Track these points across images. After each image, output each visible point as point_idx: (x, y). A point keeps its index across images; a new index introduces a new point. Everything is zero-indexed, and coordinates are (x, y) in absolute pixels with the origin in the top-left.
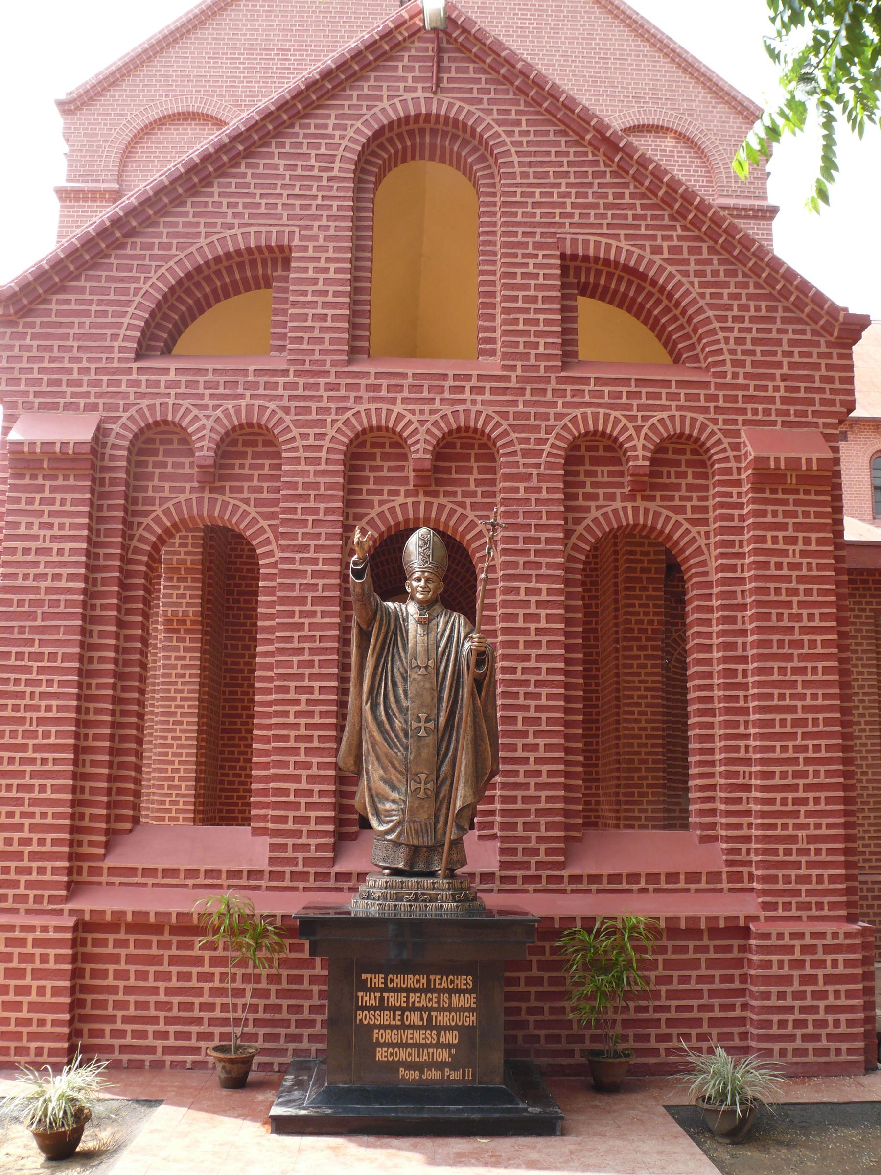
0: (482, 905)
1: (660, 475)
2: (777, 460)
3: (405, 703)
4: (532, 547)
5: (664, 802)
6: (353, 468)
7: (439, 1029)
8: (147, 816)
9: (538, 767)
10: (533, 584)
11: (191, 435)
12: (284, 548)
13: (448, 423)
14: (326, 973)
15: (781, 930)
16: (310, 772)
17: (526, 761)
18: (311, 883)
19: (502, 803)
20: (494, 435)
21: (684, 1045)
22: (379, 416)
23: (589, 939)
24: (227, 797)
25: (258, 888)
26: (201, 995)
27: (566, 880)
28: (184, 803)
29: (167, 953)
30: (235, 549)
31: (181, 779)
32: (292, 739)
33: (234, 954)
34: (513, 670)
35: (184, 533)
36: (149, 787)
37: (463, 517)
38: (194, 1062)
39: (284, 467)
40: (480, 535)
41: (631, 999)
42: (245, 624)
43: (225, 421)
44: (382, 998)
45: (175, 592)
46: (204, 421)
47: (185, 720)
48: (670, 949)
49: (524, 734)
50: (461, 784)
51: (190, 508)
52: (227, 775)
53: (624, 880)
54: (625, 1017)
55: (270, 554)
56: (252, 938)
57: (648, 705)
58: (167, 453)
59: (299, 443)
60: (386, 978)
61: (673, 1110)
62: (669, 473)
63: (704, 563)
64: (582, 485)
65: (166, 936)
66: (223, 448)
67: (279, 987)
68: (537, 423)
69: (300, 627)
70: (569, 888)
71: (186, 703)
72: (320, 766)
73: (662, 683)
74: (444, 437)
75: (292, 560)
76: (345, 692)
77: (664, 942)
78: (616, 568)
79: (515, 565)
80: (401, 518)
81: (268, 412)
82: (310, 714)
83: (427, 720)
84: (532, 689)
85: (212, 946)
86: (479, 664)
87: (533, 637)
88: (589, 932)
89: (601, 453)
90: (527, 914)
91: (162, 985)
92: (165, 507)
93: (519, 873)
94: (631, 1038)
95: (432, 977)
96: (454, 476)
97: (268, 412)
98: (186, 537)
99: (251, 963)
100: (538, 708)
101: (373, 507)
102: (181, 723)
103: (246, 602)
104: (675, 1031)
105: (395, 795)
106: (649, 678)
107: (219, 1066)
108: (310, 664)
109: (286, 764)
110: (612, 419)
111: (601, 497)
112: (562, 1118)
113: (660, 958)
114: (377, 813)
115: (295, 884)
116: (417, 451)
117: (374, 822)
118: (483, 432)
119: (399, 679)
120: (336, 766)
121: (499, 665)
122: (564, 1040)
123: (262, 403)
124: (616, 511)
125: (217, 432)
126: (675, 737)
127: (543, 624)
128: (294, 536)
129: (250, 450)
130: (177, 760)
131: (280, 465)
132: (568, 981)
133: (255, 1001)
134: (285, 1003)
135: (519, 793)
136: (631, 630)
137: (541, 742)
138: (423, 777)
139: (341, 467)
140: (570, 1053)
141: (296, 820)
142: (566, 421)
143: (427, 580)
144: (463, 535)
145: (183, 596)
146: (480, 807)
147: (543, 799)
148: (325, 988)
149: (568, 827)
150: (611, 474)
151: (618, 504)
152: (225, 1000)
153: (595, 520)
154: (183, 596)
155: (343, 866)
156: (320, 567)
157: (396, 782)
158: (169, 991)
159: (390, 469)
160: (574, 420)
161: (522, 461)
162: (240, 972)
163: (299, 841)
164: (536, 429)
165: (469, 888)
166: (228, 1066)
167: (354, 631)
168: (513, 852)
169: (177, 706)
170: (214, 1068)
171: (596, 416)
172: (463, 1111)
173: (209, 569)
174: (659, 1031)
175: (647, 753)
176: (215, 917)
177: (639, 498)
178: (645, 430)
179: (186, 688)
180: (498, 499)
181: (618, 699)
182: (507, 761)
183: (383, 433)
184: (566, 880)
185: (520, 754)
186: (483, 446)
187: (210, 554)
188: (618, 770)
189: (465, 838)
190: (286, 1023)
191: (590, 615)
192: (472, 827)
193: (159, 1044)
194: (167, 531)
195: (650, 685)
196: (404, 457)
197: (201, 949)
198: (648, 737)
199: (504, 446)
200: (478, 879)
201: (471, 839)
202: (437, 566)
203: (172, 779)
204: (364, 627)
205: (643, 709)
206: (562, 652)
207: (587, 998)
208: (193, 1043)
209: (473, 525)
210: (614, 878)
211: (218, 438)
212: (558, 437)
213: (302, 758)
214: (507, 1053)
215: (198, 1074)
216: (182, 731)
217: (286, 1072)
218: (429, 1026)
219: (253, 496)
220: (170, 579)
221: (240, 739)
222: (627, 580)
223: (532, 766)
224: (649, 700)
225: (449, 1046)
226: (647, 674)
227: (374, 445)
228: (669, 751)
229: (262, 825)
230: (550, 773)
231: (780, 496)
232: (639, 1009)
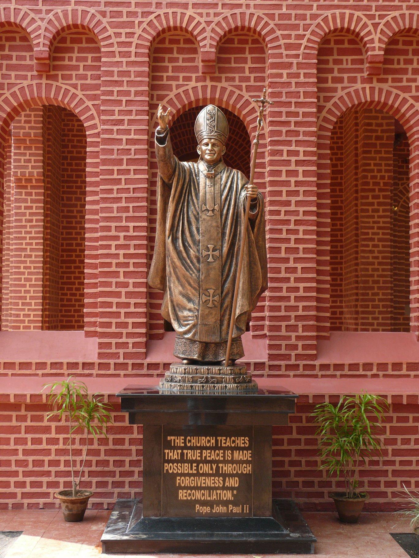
0: (255, 386)
1: (391, 62)
3: (197, 237)
4: (293, 119)
5: (391, 312)
6: (156, 60)
7: (225, 476)
8: (6, 326)
9: (297, 285)
10: (293, 148)
11: (29, 34)
12: (104, 122)
13: (228, 23)
14: (141, 436)
17: (288, 280)
18: (130, 371)
19: (270, 311)
20: (263, 33)
21: (406, 490)
22: (175, 18)
23: (335, 411)
24: (66, 311)
26: (50, 455)
27: (317, 368)
28: (35, 316)
29: (23, 424)
30: (68, 125)
31: (32, 298)
32: (114, 265)
33: (73, 424)
34: (278, 213)
35: (28, 112)
36: (7, 304)
37: (240, 97)
38: (45, 504)
39: (103, 59)
40: (253, 110)
41: (367, 456)
42: (76, 182)
43: (56, 23)
44: (182, 454)
45: (23, 158)
46: (39, 23)
47: (34, 254)
48: (395, 419)
49: (287, 260)
50: (240, 297)
51: (31, 92)
52: (66, 294)
53: (361, 368)
54: (361, 468)
55: (94, 126)
56: (86, 412)
57: (380, 240)
58: (11, 48)
59: (114, 40)
60: (185, 440)
61: (397, 537)
62: (399, 60)
64: (331, 71)
65: (23, 412)
66: (56, 44)
67: (107, 448)
68: (297, 22)
69: (118, 181)
70: (320, 373)
71: (34, 242)
72: (135, 285)
73: (391, 223)
74: (225, 35)
75: (111, 131)
76: (153, 230)
77: (391, 414)
78: (357, 136)
79: (279, 133)
80: (193, 99)
81: (89, 15)
82: (127, 247)
83: (214, 250)
84: (292, 227)
85: (56, 418)
86: (253, 207)
87: (293, 188)
88: (335, 405)
89: (346, 45)
90: (289, 392)
91: (20, 448)
92: (12, 91)
93: (283, 363)
94: (366, 484)
95: (219, 438)
96: (233, 65)
97: (89, 15)
98: (30, 116)
99: (86, 430)
100: (297, 241)
101: (171, 90)
102: (31, 256)
103: (77, 165)
104: (399, 480)
105: (190, 305)
106: (381, 220)
107: (64, 506)
108: (126, 209)
109: (109, 284)
110: (355, 18)
111: (346, 80)
112: (315, 541)
113: (388, 425)
114: (178, 319)
115: (117, 372)
116: (205, 46)
117: (175, 325)
118: (255, 30)
119: (193, 219)
120: (147, 285)
121: (268, 208)
122: (316, 485)
123: (84, 8)
124: (356, 91)
125: (50, 32)
126: (400, 264)
127: (301, 178)
128: (112, 113)
129: (76, 46)
130: (28, 283)
131: (100, 58)
132: (319, 442)
133: (89, 458)
134: (111, 459)
135: (283, 304)
136: (367, 184)
137: (299, 266)
138: (211, 291)
139: (147, 59)
140: (321, 495)
141: (118, 325)
142: (319, 20)
143: (213, 145)
144: (240, 111)
145: (29, 161)
146: (254, 315)
147: (301, 308)
148: (141, 447)
149: (319, 329)
150: (353, 62)
151: (359, 86)
152: (67, 458)
153: (341, 98)
154: (29, 161)
155: (152, 359)
156: (132, 136)
157: (191, 296)
158: (26, 452)
159: (184, 60)
160: (325, 20)
161: (285, 53)
162: (78, 437)
163: (121, 341)
164: (296, 27)
165: (246, 374)
166: (70, 506)
167: (159, 184)
168: (279, 347)
169: (27, 244)
170: (60, 507)
171: (342, 16)
172: (242, 536)
173: (48, 140)
174: (387, 479)
176: (59, 397)
177: (375, 80)
178: (381, 27)
179: (33, 230)
180: (267, 83)
181: (357, 235)
182: (273, 280)
183: (178, 32)
184: (317, 368)
185: (283, 275)
186: (255, 41)
187: (48, 129)
188: (357, 288)
189: (242, 336)
190: (112, 474)
191: (336, 172)
192: (248, 329)
193: (19, 491)
194: (14, 109)
195: (381, 225)
196: (195, 51)
197: (49, 420)
198: (380, 264)
199: (272, 41)
200: (252, 367)
201: (247, 338)
202: (220, 134)
203: (25, 298)
204: (166, 181)
205: (376, 242)
206: (315, 198)
207: (334, 454)
208: (44, 489)
209: (247, 103)
210: (354, 366)
211: (51, 36)
212: (313, 33)
213: (122, 279)
214: (274, 494)
215: (47, 512)
216: (31, 262)
217: (113, 509)
218: (217, 474)
219: (80, 82)
220: (19, 148)
221: (76, 268)
222: (365, 145)
223: (292, 284)
224: (381, 236)
225: (232, 489)
226: (379, 217)
227: (171, 41)
228: (396, 274)
229: (92, 329)
230: (306, 289)
232: (372, 463)
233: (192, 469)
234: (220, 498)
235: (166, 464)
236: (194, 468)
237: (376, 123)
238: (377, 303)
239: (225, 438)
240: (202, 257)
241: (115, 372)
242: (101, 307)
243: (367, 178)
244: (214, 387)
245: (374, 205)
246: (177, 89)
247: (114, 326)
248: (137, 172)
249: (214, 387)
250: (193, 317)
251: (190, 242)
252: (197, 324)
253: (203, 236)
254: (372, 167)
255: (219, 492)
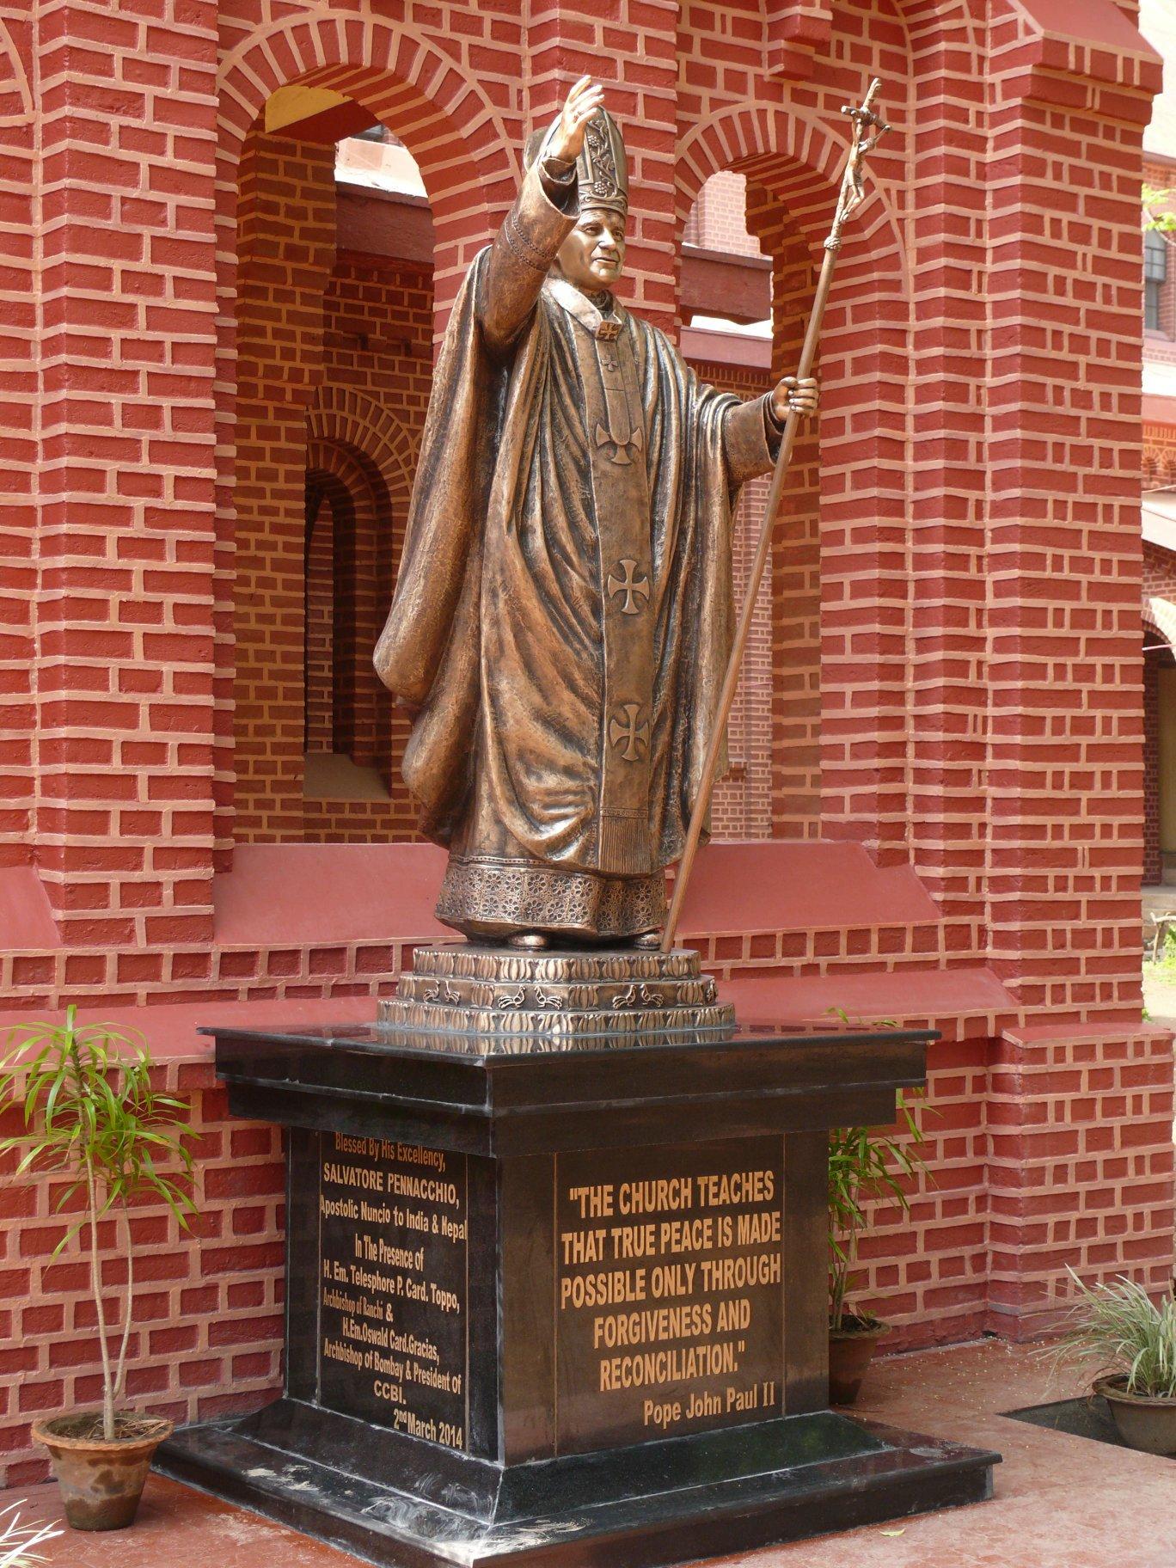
2: (1080, 50)
3: (590, 533)
7: (717, 1298)
15: (1060, 1042)
16: (157, 698)
18: (167, 982)
25: (38, 1002)
44: (609, 1241)
60: (615, 1194)
63: (893, 262)
95: (702, 1181)
108: (150, 416)
115: (127, 987)
138: (632, 709)
150: (741, 27)
163: (136, 877)
175: (274, 675)
213: (138, 661)
218: (698, 1296)
225: (733, 1336)
231: (1067, 133)
233: (633, 1290)
234: (705, 1371)
235: (566, 1281)
236: (640, 1283)
237: (288, 207)
238: (269, 757)
239: (715, 1178)
240: (607, 595)
241: (118, 989)
242: (72, 759)
243: (280, 377)
244: (665, 1017)
245: (262, 458)
246: (274, 18)
247: (114, 824)
248: (185, 286)
249: (665, 1017)
250: (583, 792)
251: (570, 548)
252: (595, 816)
253: (606, 528)
254: (269, 341)
255: (701, 1350)
